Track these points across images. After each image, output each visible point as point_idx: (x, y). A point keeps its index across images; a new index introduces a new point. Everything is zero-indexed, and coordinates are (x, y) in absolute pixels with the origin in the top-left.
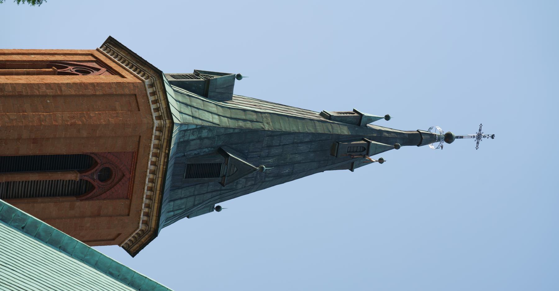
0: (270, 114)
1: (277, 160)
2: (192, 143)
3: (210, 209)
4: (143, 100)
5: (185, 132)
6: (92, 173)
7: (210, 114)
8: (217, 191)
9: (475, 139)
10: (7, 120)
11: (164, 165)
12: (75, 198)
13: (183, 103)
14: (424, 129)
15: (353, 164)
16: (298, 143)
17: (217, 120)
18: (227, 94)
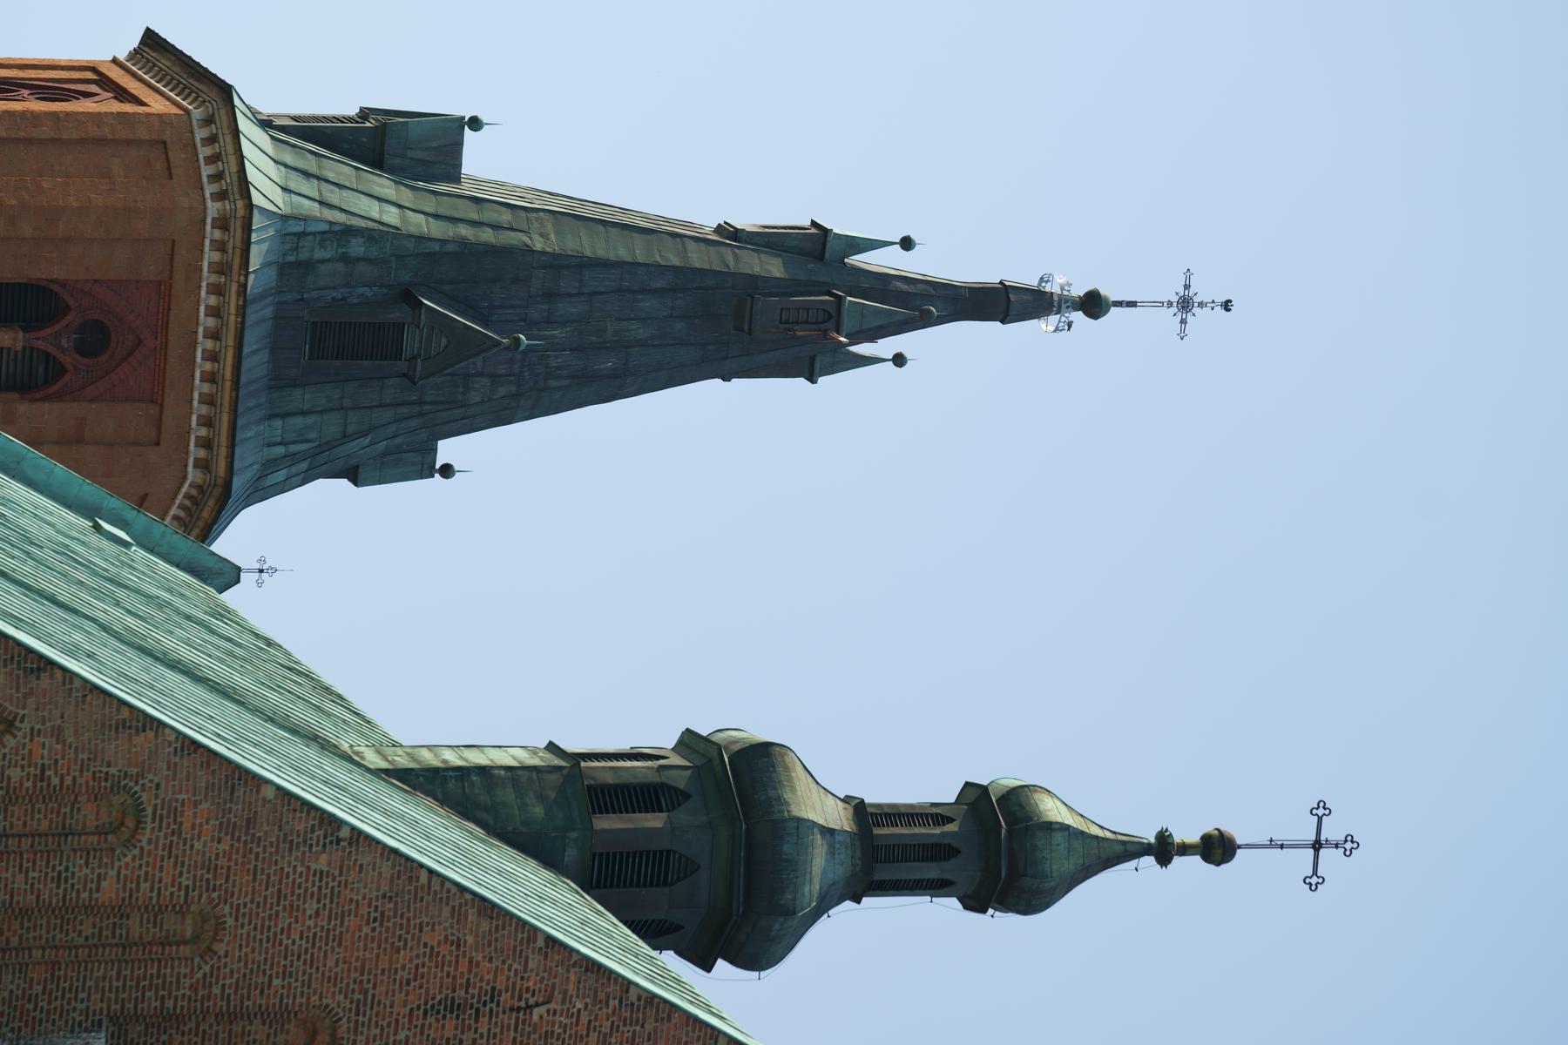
0: (554, 215)
1: (576, 333)
2: (323, 268)
4: (183, 156)
5: (298, 239)
6: (56, 332)
7: (376, 203)
8: (412, 403)
9: (1174, 309)
11: (236, 315)
12: (16, 396)
13: (295, 169)
14: (1024, 276)
15: (812, 359)
16: (633, 292)
17: (395, 217)
18: (444, 166)
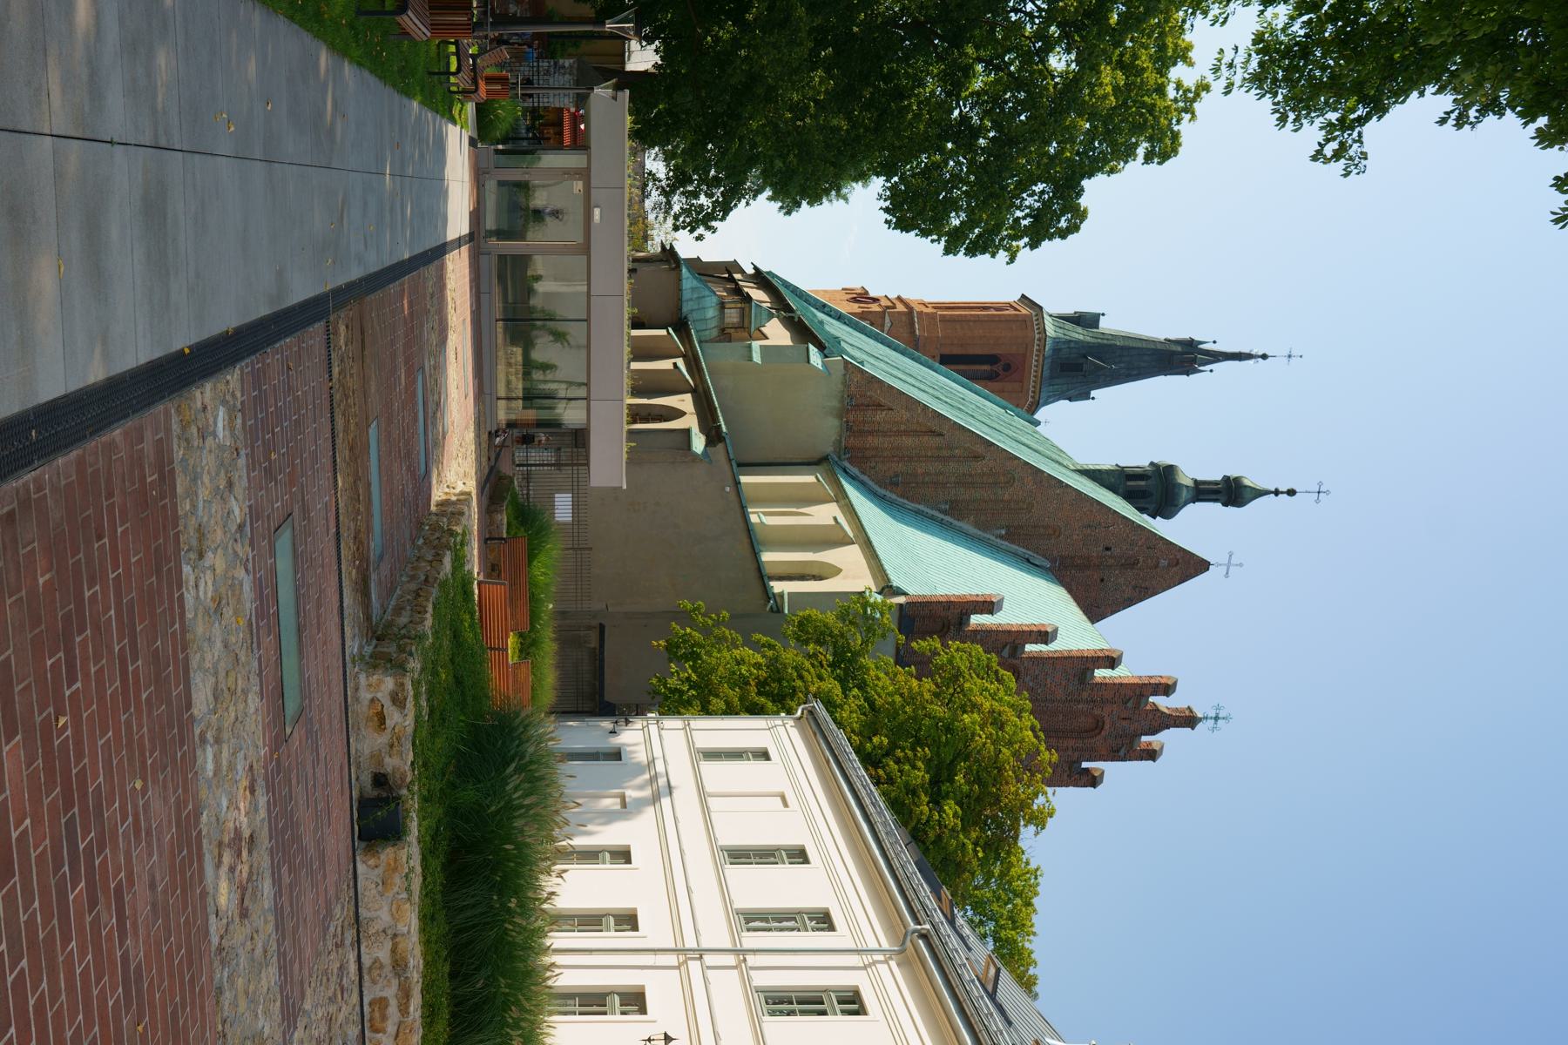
3: (1086, 396)
14: (1246, 350)
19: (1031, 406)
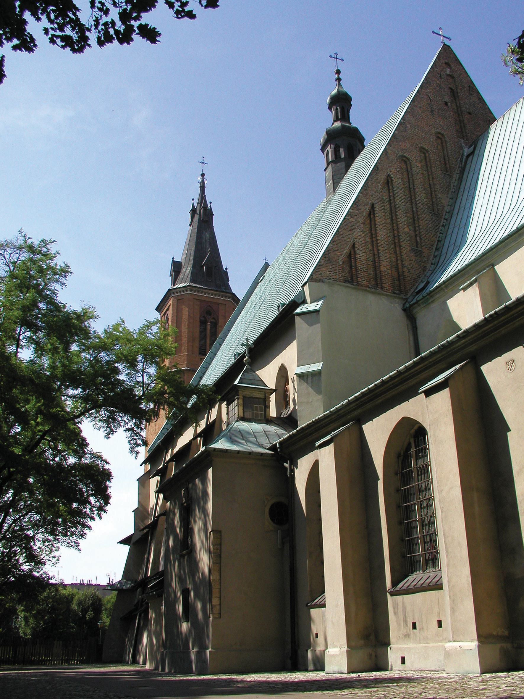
3: (226, 272)
10: (184, 351)
14: (199, 185)
19: (234, 300)
